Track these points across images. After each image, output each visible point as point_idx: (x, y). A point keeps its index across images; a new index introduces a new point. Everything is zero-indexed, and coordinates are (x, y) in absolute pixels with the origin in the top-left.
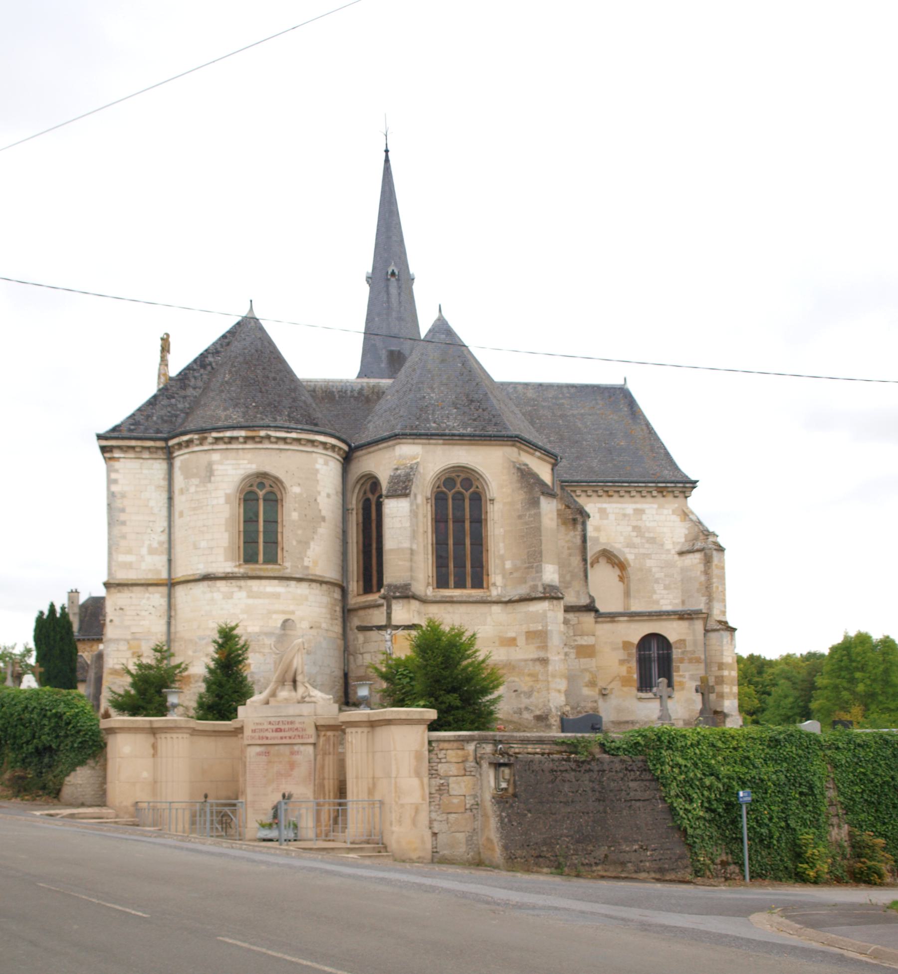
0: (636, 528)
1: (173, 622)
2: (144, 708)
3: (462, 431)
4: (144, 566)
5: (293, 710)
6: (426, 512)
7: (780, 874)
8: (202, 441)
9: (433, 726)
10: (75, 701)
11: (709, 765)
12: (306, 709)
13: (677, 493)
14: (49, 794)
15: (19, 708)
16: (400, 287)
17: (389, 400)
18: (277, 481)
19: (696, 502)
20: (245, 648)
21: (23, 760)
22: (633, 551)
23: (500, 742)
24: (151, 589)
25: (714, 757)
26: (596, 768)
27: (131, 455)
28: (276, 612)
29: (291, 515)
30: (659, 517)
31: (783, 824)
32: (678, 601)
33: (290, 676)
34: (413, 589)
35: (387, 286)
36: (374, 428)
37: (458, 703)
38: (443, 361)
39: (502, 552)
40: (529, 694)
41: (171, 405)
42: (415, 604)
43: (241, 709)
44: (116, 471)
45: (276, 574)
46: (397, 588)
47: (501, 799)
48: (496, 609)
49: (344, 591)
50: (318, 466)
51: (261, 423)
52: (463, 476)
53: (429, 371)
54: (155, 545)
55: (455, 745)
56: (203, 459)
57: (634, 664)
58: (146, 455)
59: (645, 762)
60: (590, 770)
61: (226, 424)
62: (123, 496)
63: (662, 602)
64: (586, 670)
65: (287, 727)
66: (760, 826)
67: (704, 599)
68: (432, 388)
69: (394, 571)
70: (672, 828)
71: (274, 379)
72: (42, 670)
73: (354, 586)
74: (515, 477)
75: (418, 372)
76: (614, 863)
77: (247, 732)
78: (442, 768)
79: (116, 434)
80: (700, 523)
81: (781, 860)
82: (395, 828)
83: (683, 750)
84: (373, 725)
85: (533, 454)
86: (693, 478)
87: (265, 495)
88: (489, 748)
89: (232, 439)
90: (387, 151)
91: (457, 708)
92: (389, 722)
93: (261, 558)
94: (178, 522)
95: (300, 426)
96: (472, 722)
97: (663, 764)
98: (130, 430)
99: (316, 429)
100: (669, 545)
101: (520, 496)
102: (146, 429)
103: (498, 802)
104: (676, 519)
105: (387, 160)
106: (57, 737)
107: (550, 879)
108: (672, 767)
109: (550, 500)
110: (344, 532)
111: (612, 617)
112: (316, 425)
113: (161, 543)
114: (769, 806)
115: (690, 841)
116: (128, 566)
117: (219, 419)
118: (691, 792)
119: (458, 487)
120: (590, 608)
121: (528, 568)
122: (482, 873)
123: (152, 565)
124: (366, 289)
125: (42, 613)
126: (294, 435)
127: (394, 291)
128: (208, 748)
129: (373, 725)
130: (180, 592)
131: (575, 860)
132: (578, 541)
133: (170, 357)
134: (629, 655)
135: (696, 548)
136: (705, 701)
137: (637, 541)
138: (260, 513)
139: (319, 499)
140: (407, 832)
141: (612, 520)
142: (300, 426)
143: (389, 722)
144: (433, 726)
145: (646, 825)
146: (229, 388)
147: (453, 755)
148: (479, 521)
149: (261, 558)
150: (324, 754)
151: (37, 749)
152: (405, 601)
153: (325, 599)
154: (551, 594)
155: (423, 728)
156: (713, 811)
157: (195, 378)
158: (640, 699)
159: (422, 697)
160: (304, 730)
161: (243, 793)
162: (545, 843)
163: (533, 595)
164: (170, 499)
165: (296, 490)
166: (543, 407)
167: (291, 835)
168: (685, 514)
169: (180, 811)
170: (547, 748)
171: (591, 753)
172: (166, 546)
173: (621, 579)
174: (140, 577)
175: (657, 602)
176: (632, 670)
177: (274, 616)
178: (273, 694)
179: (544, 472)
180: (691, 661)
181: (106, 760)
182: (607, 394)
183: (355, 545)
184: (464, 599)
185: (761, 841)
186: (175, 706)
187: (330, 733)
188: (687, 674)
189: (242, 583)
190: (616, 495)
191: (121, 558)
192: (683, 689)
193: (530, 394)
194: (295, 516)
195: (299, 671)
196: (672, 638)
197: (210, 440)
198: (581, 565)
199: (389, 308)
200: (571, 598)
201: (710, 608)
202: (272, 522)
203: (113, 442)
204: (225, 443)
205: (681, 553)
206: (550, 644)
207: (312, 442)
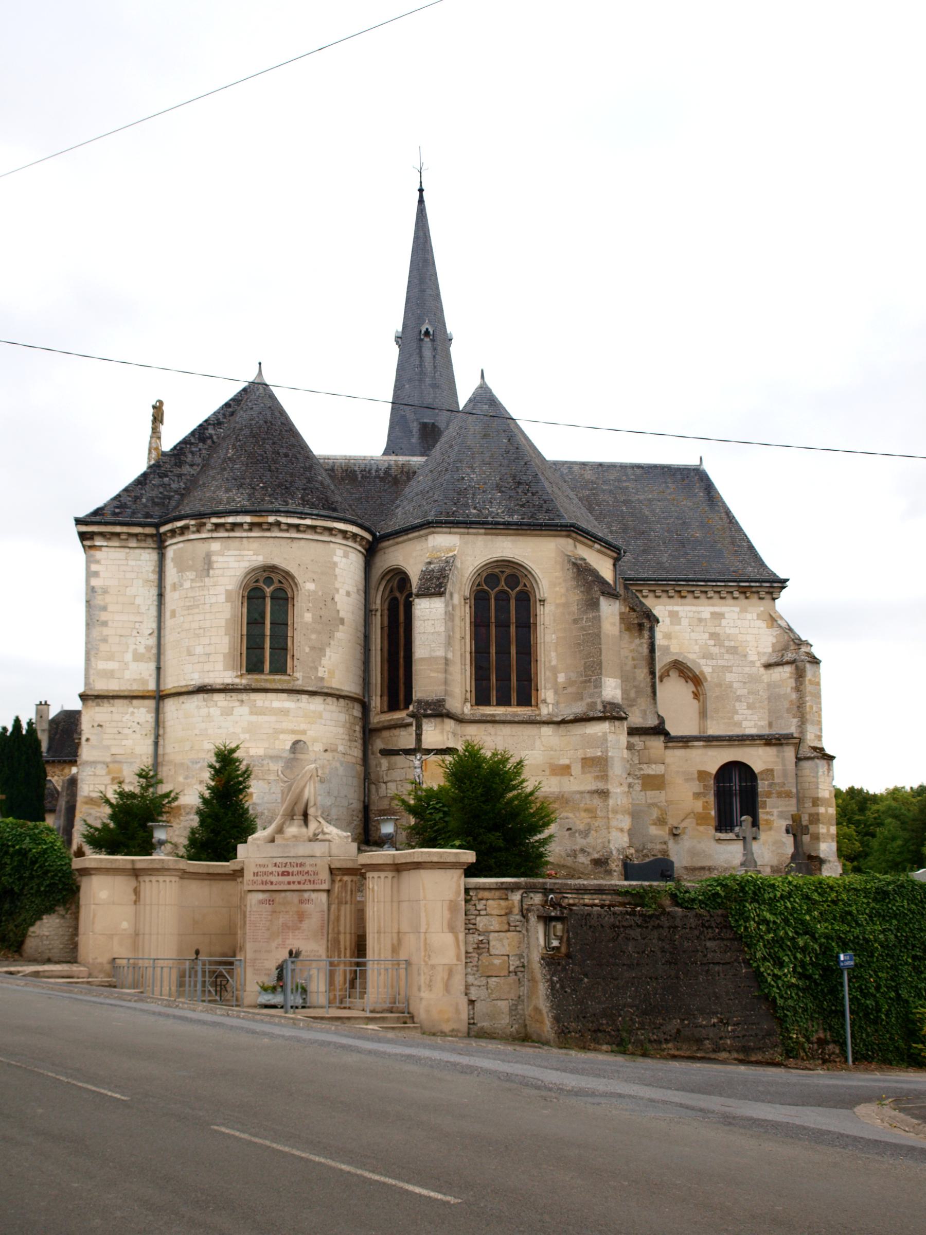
0: (713, 636)
1: (161, 742)
2: (127, 846)
3: (507, 519)
4: (128, 675)
5: (303, 849)
7: (890, 1056)
8: (200, 528)
9: (471, 871)
10: (44, 836)
11: (803, 922)
12: (318, 849)
13: (762, 594)
16: (435, 349)
17: (421, 482)
18: (287, 575)
19: (785, 603)
20: (247, 773)
23: (552, 891)
24: (135, 702)
25: (809, 912)
26: (667, 924)
27: (115, 543)
29: (303, 615)
30: (741, 625)
31: (893, 994)
32: (764, 723)
33: (300, 809)
34: (447, 706)
35: (420, 348)
37: (501, 843)
38: (485, 436)
39: (554, 663)
40: (586, 834)
41: (164, 485)
42: (450, 724)
43: (240, 847)
45: (285, 687)
46: (428, 704)
47: (552, 960)
48: (546, 730)
50: (336, 559)
51: (270, 507)
52: (508, 571)
53: (469, 448)
54: (142, 650)
55: (497, 894)
57: (711, 799)
58: (133, 543)
59: (725, 917)
62: (105, 591)
63: (745, 724)
64: (654, 805)
65: (295, 869)
67: (795, 721)
68: (472, 468)
69: (425, 685)
70: (758, 997)
71: (286, 455)
73: (376, 702)
74: (570, 574)
75: (456, 448)
77: (248, 876)
79: (97, 519)
80: (790, 629)
82: (424, 994)
84: (398, 868)
85: (591, 547)
88: (537, 898)
89: (235, 526)
90: (421, 190)
91: (500, 849)
93: (494, 700)
94: (169, 622)
97: (747, 919)
98: (115, 514)
99: (335, 514)
100: (753, 657)
101: (576, 597)
102: (134, 513)
103: (548, 964)
104: (762, 624)
105: (421, 201)
106: (21, 878)
108: (758, 924)
109: (611, 601)
110: (367, 638)
111: (685, 741)
112: (335, 510)
113: (148, 648)
114: (875, 972)
115: (780, 1014)
116: (110, 674)
118: (781, 954)
120: (659, 730)
121: (585, 682)
122: (527, 1051)
123: (140, 675)
124: (395, 350)
126: (308, 522)
128: (202, 894)
129: (398, 868)
130: (171, 707)
132: (645, 650)
134: (705, 787)
135: (786, 659)
136: (797, 843)
137: (715, 650)
138: (267, 605)
139: (337, 598)
140: (439, 998)
141: (684, 625)
144: (471, 871)
146: (237, 462)
147: (494, 906)
148: (527, 626)
149: (494, 700)
152: (438, 720)
153: (343, 717)
154: (612, 714)
155: (460, 872)
157: (193, 453)
158: (719, 840)
159: (457, 836)
163: (591, 714)
164: (161, 596)
165: (310, 586)
166: (604, 491)
168: (773, 620)
170: (607, 899)
171: (661, 906)
172: (154, 651)
173: (696, 696)
174: (123, 688)
175: (739, 724)
176: (708, 805)
177: (282, 736)
178: (280, 830)
179: (605, 568)
180: (779, 795)
181: (78, 907)
183: (379, 652)
184: (509, 718)
186: (162, 843)
187: (346, 878)
189: (244, 696)
190: (690, 596)
191: (102, 665)
192: (770, 829)
193: (589, 475)
194: (308, 617)
195: (311, 803)
196: (757, 767)
197: (209, 526)
199: (422, 373)
200: (636, 719)
202: (282, 625)
203: (95, 528)
204: (227, 530)
205: (768, 666)
206: (610, 773)
207: (330, 530)
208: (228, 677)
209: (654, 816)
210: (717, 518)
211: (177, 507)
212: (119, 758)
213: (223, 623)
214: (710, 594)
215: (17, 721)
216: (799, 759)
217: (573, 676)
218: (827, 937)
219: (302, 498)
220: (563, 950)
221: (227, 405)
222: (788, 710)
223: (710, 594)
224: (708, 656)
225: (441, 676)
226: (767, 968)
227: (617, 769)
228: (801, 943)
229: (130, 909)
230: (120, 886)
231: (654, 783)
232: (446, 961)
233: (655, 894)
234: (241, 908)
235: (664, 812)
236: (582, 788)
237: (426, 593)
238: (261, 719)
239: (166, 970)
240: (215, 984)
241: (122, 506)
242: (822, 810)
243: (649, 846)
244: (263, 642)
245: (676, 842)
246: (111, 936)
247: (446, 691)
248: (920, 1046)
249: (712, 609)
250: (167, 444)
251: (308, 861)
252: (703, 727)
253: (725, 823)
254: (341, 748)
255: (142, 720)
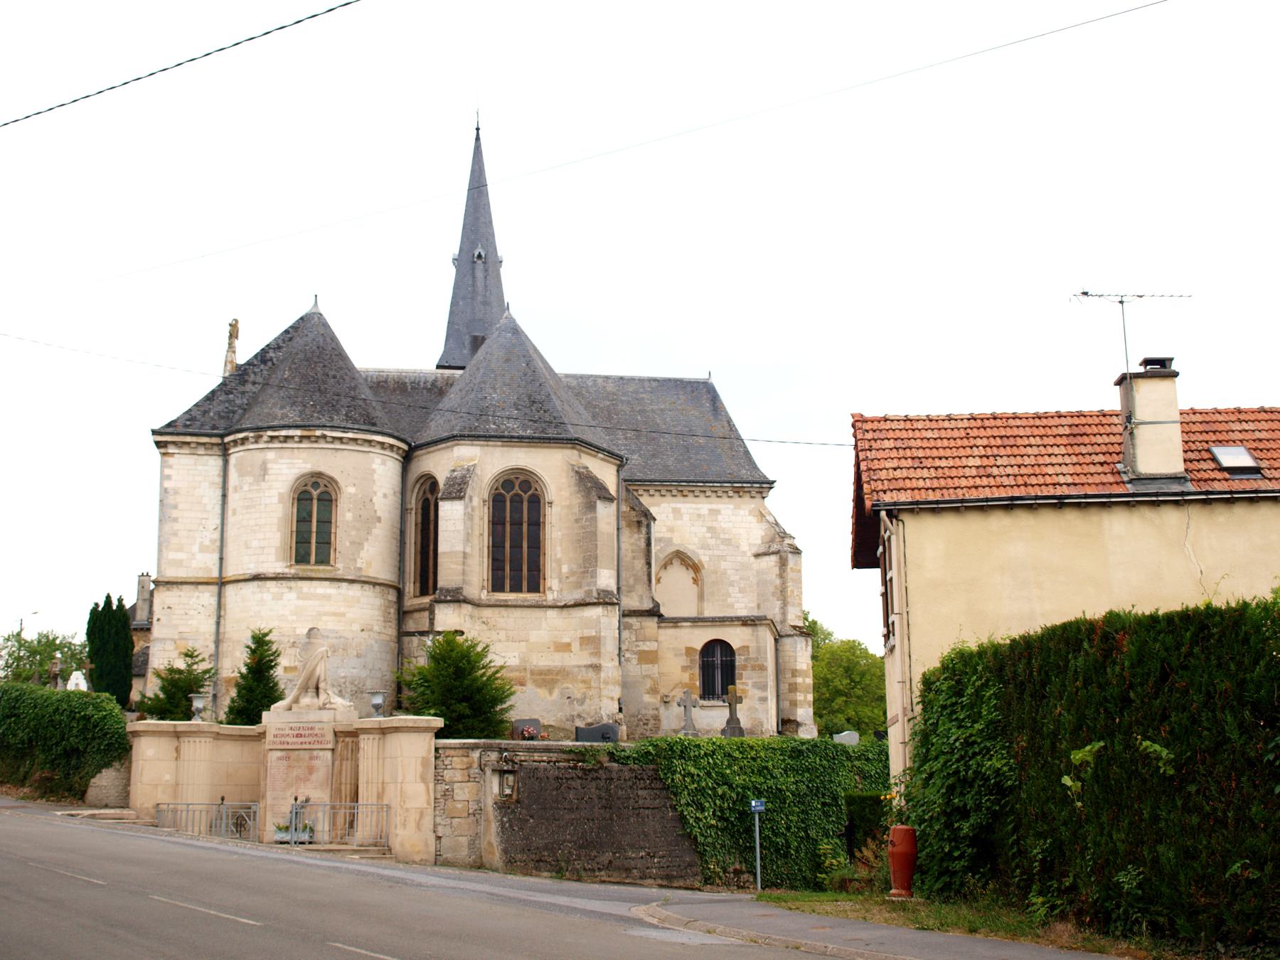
0: (710, 529)
1: (222, 622)
2: (170, 712)
3: (521, 433)
4: (194, 564)
5: (314, 716)
6: (482, 516)
7: (798, 883)
8: (257, 439)
9: (440, 734)
10: (104, 704)
11: (723, 775)
12: (326, 716)
13: (754, 494)
14: (75, 795)
15: (50, 710)
16: (486, 271)
17: (452, 399)
18: (332, 480)
19: (773, 501)
20: (277, 654)
21: (53, 761)
22: (707, 552)
23: (506, 750)
24: (200, 587)
25: (729, 766)
26: (604, 776)
27: (186, 450)
28: (326, 614)
29: (345, 515)
31: (802, 834)
32: (754, 605)
33: (312, 684)
34: (465, 593)
35: (473, 269)
36: (437, 426)
37: (468, 712)
38: (507, 360)
39: (559, 556)
40: (582, 701)
41: (229, 401)
42: (467, 608)
43: (265, 714)
44: (170, 467)
45: (328, 576)
46: (448, 591)
47: (504, 805)
48: (551, 613)
49: (400, 593)
50: (375, 466)
51: (317, 422)
52: (522, 478)
53: (493, 371)
54: (207, 543)
55: (461, 752)
56: (259, 456)
58: (201, 451)
59: (656, 771)
60: (597, 778)
61: (282, 423)
62: (176, 492)
63: (737, 606)
64: (648, 676)
66: (776, 835)
67: (778, 603)
68: (494, 389)
69: (447, 575)
70: (682, 836)
71: (334, 377)
72: (93, 666)
73: (410, 588)
74: (573, 481)
75: (482, 371)
76: (618, 868)
77: (269, 737)
78: (448, 775)
79: (170, 430)
80: (777, 524)
81: (800, 870)
82: (400, 831)
83: (696, 760)
84: (383, 731)
86: (771, 478)
87: (319, 495)
88: (494, 756)
89: (287, 438)
90: (478, 129)
91: (468, 717)
92: (397, 730)
93: (507, 587)
94: (231, 519)
95: (356, 426)
96: (482, 730)
97: (674, 772)
98: (186, 426)
99: (373, 429)
100: (744, 547)
101: (577, 500)
102: (202, 425)
103: (499, 808)
104: (753, 520)
105: (478, 139)
106: (85, 739)
107: (548, 881)
108: (684, 776)
109: (607, 504)
110: (402, 533)
111: (675, 622)
112: (374, 424)
113: (212, 541)
114: (787, 816)
115: (700, 849)
116: (179, 563)
117: (275, 418)
118: (702, 801)
119: (517, 490)
120: (654, 612)
122: (481, 875)
123: (205, 565)
124: (452, 271)
125: (97, 605)
126: (350, 435)
127: (480, 274)
128: (232, 753)
129: (383, 731)
130: (230, 590)
131: (578, 865)
132: (643, 544)
133: (237, 343)
134: (692, 661)
135: (772, 549)
137: (712, 542)
138: (313, 509)
139: (375, 500)
140: (411, 835)
141: (679, 520)
142: (356, 426)
143: (397, 730)
144: (440, 734)
145: (655, 832)
146: (289, 383)
147: (458, 761)
148: (537, 524)
149: (507, 587)
150: (342, 760)
151: (65, 750)
152: (456, 605)
153: (378, 602)
154: (605, 600)
155: (431, 735)
156: (727, 820)
157: (255, 373)
159: (434, 705)
160: (323, 736)
161: (264, 797)
162: (546, 848)
163: (588, 600)
164: (224, 496)
165: (352, 490)
166: (622, 402)
167: (305, 837)
168: (762, 516)
169: (197, 813)
170: (554, 756)
171: (600, 762)
172: (218, 543)
173: (695, 581)
174: (190, 575)
175: (732, 606)
176: (694, 677)
177: (324, 618)
178: (296, 701)
179: (607, 474)
180: (753, 668)
181: (130, 763)
182: (689, 389)
184: (519, 603)
185: (775, 851)
186: (199, 711)
187: (347, 739)
188: (750, 682)
189: (293, 584)
190: (691, 495)
191: (172, 555)
193: (610, 387)
194: (349, 516)
195: (322, 678)
196: (735, 645)
197: (265, 438)
198: (645, 569)
199: (474, 291)
201: (784, 614)
202: (326, 522)
203: (171, 436)
205: (757, 556)
206: (603, 650)
208: (279, 567)
209: (648, 686)
210: (635, 459)
211: (239, 421)
212: (185, 635)
213: (276, 521)
214: (708, 493)
215: (108, 597)
216: (778, 638)
217: (574, 567)
218: (744, 788)
219: (346, 415)
220: (515, 797)
221: (286, 332)
222: (773, 595)
223: (708, 493)
224: (705, 546)
225: (460, 567)
226: (690, 812)
227: (610, 647)
228: (720, 791)
229: (173, 764)
230: (166, 745)
231: (649, 658)
232: (418, 805)
233: (594, 753)
234: (262, 763)
235: (656, 683)
236: (580, 663)
237: (449, 497)
238: (306, 603)
239: (204, 814)
240: (236, 825)
241: (193, 419)
242: (799, 680)
243: (643, 712)
244: (310, 538)
245: (667, 708)
246: (156, 786)
247: (464, 581)
248: (824, 876)
249: (709, 506)
250: (243, 357)
251: (317, 726)
252: (700, 610)
253: (708, 691)
254: (376, 628)
255: (206, 603)
